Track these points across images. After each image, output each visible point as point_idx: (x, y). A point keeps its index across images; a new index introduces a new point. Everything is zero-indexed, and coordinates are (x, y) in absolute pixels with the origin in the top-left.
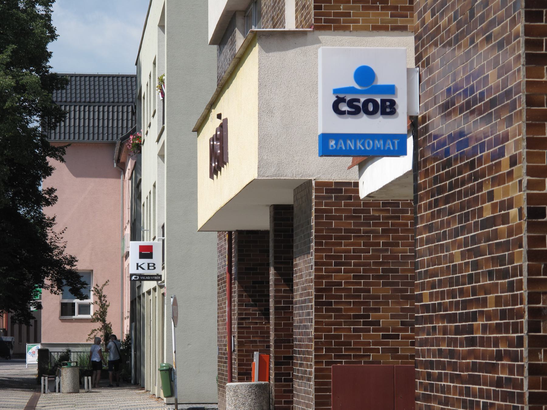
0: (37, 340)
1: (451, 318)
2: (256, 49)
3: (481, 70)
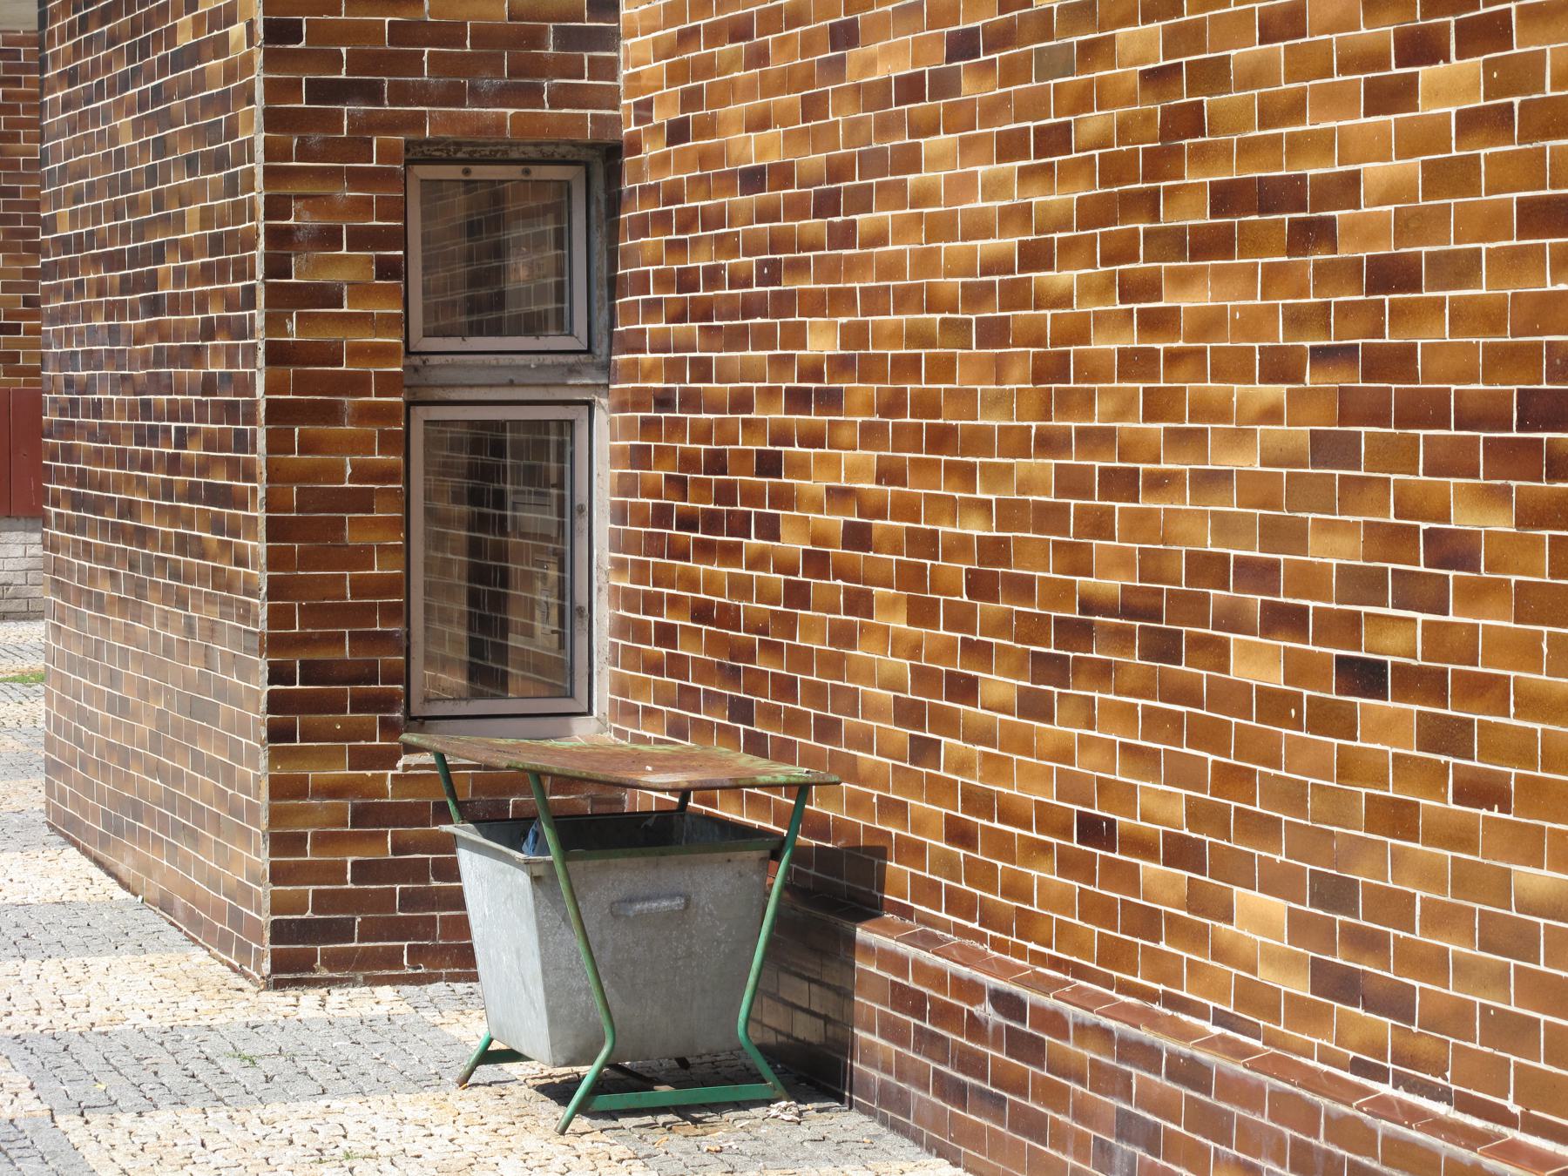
1: (114, 261)
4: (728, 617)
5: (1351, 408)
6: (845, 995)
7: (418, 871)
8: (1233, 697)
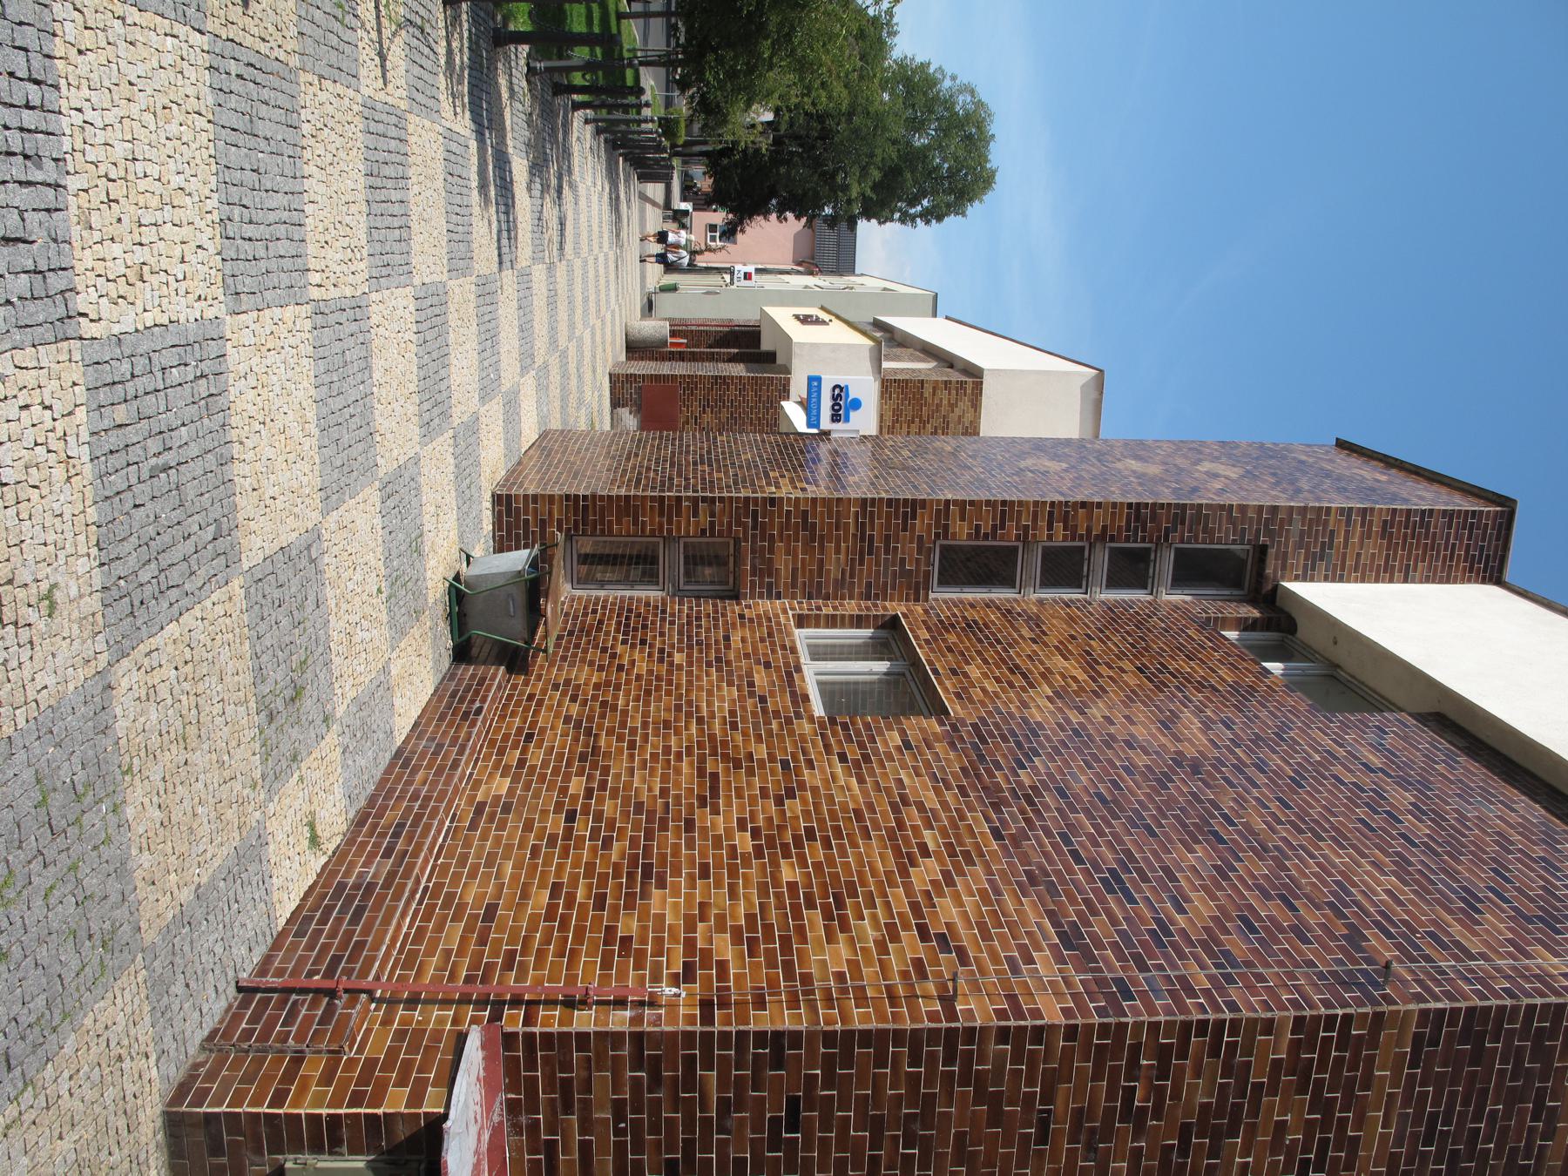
0: (694, 209)
1: (709, 452)
2: (871, 343)
3: (858, 473)
4: (599, 630)
5: (651, 815)
6: (484, 663)
7: (527, 537)
8: (567, 777)
